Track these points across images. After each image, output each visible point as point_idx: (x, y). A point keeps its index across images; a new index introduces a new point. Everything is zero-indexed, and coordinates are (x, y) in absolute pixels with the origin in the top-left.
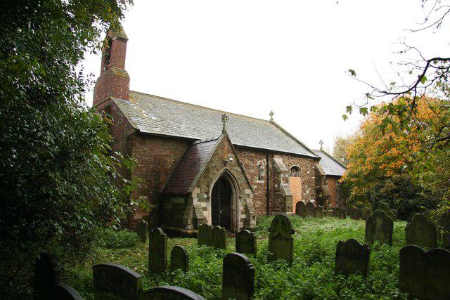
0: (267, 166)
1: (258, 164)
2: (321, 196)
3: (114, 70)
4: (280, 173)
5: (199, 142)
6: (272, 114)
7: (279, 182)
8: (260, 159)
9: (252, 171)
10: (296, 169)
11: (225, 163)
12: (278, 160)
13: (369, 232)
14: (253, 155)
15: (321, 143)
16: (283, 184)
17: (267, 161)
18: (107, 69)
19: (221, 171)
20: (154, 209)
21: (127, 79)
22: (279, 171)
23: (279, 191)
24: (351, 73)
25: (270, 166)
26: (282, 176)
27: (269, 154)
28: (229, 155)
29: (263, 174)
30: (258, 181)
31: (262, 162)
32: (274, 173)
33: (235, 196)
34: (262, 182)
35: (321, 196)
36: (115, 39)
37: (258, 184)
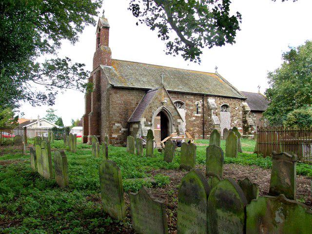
0: (203, 105)
1: (196, 103)
2: (246, 125)
3: (102, 48)
4: (211, 109)
5: (150, 91)
6: (216, 68)
7: (210, 115)
8: (198, 100)
9: (191, 108)
10: (226, 106)
11: (162, 103)
12: (211, 101)
13: (193, 153)
14: (193, 97)
15: (39, 116)
16: (214, 117)
17: (203, 101)
18: (98, 47)
19: (160, 108)
20: (124, 131)
21: (110, 53)
22: (211, 108)
23: (211, 121)
24: (169, 54)
25: (206, 105)
26: (213, 111)
27: (204, 96)
28: (165, 98)
29: (200, 110)
30: (196, 115)
31: (199, 102)
32: (207, 110)
33: (170, 124)
34: (199, 115)
35: (246, 125)
36: (101, 28)
37: (196, 117)
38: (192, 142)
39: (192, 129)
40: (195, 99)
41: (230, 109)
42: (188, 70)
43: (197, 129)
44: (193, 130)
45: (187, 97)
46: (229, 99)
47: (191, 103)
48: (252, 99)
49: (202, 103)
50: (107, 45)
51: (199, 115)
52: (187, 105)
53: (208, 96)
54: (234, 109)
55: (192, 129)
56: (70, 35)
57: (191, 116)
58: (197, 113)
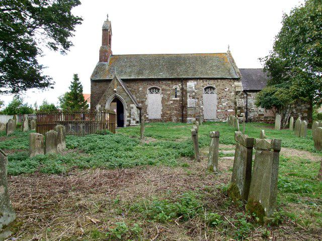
1: (174, 88)
9: (168, 92)
14: (170, 82)
19: (113, 96)
34: (178, 99)
38: (11, 89)
39: (169, 112)
40: (172, 84)
41: (216, 90)
42: (192, 54)
43: (175, 112)
44: (171, 113)
45: (164, 82)
46: (216, 81)
47: (168, 88)
48: (246, 75)
49: (181, 86)
50: (110, 47)
51: (178, 99)
52: (163, 90)
53: (187, 79)
54: (223, 90)
55: (169, 112)
56: (25, 90)
57: (168, 100)
58: (176, 97)
